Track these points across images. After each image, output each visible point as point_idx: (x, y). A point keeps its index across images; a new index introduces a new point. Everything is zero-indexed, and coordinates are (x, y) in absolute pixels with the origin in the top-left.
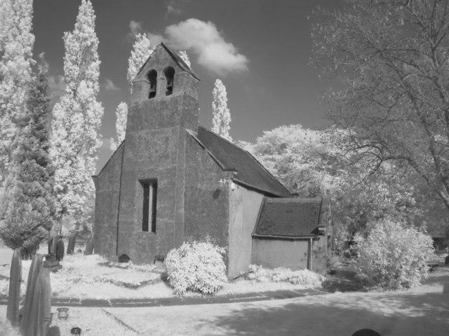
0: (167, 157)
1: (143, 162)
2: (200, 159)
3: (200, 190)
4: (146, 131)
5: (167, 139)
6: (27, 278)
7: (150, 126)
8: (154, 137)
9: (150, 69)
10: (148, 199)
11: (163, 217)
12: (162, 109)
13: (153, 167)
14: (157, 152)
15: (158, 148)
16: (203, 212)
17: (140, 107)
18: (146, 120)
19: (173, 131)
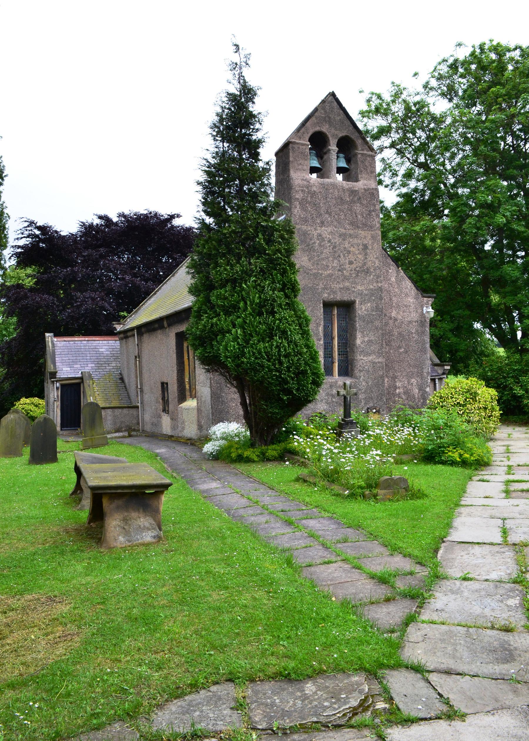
0: (367, 272)
1: (330, 276)
2: (393, 279)
3: (396, 320)
4: (330, 229)
5: (365, 247)
6: (104, 505)
7: (335, 223)
8: (344, 240)
9: (317, 129)
10: (184, 368)
11: (368, 354)
12: (353, 202)
13: (347, 284)
14: (351, 263)
15: (351, 257)
16: (400, 347)
17: (314, 189)
18: (327, 212)
19: (372, 237)
